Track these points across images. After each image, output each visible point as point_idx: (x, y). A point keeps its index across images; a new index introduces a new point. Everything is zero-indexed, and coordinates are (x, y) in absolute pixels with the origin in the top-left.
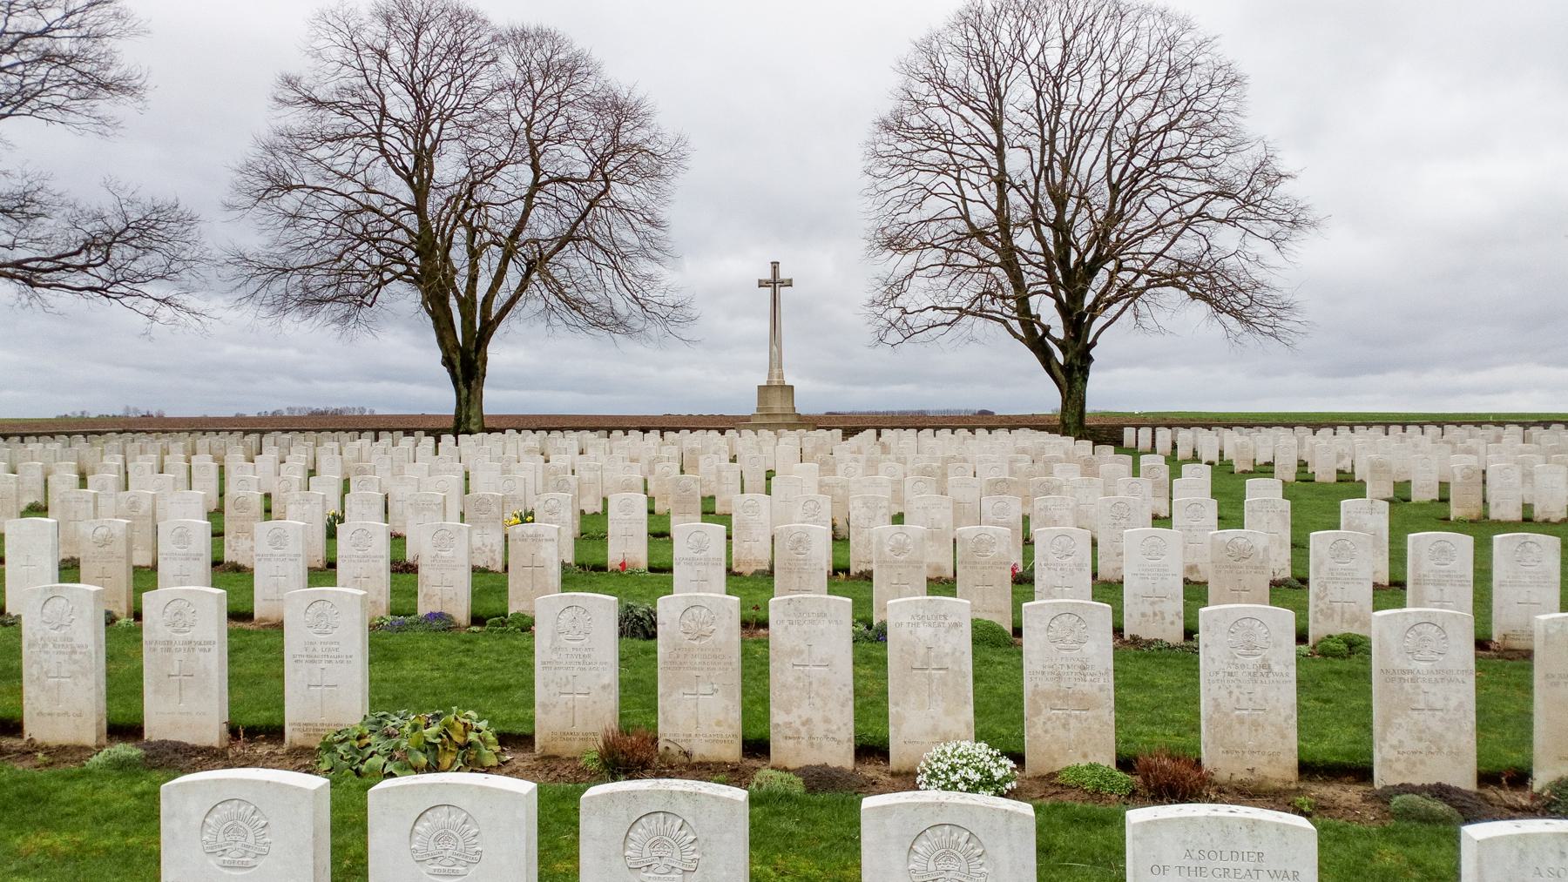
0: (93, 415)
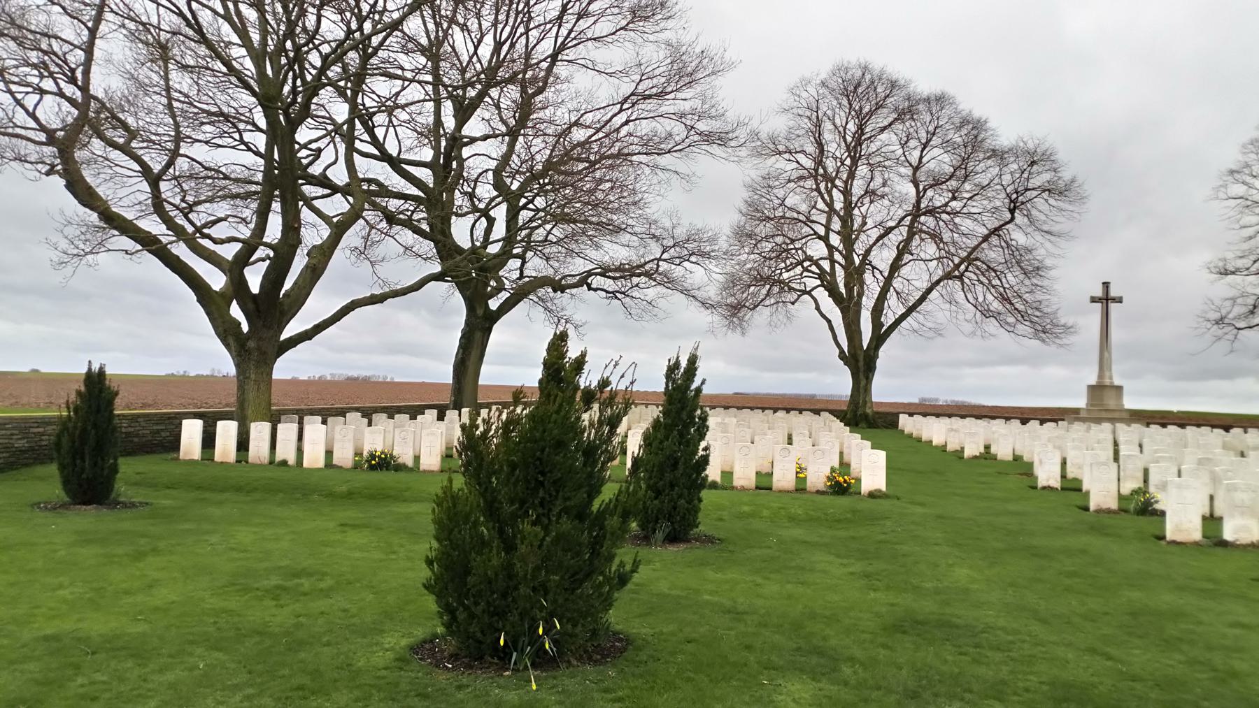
0: (192, 374)
